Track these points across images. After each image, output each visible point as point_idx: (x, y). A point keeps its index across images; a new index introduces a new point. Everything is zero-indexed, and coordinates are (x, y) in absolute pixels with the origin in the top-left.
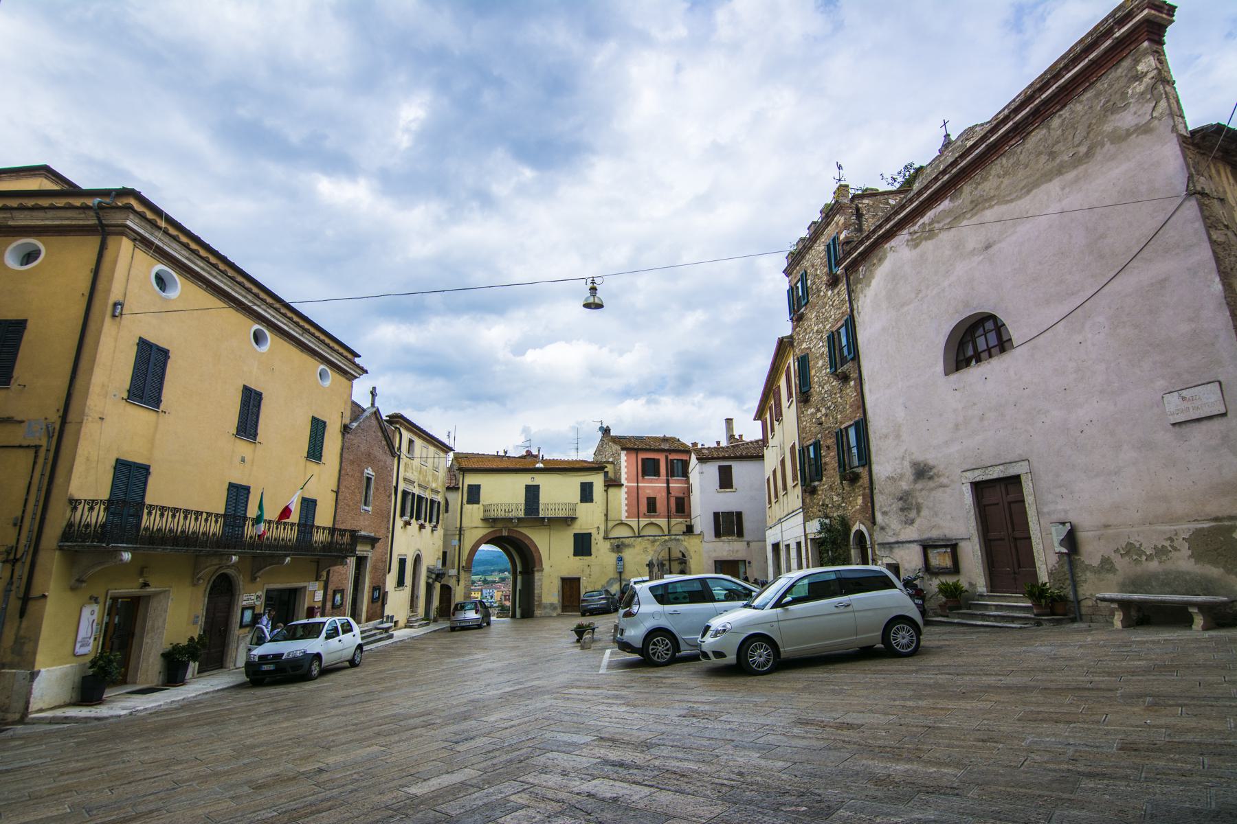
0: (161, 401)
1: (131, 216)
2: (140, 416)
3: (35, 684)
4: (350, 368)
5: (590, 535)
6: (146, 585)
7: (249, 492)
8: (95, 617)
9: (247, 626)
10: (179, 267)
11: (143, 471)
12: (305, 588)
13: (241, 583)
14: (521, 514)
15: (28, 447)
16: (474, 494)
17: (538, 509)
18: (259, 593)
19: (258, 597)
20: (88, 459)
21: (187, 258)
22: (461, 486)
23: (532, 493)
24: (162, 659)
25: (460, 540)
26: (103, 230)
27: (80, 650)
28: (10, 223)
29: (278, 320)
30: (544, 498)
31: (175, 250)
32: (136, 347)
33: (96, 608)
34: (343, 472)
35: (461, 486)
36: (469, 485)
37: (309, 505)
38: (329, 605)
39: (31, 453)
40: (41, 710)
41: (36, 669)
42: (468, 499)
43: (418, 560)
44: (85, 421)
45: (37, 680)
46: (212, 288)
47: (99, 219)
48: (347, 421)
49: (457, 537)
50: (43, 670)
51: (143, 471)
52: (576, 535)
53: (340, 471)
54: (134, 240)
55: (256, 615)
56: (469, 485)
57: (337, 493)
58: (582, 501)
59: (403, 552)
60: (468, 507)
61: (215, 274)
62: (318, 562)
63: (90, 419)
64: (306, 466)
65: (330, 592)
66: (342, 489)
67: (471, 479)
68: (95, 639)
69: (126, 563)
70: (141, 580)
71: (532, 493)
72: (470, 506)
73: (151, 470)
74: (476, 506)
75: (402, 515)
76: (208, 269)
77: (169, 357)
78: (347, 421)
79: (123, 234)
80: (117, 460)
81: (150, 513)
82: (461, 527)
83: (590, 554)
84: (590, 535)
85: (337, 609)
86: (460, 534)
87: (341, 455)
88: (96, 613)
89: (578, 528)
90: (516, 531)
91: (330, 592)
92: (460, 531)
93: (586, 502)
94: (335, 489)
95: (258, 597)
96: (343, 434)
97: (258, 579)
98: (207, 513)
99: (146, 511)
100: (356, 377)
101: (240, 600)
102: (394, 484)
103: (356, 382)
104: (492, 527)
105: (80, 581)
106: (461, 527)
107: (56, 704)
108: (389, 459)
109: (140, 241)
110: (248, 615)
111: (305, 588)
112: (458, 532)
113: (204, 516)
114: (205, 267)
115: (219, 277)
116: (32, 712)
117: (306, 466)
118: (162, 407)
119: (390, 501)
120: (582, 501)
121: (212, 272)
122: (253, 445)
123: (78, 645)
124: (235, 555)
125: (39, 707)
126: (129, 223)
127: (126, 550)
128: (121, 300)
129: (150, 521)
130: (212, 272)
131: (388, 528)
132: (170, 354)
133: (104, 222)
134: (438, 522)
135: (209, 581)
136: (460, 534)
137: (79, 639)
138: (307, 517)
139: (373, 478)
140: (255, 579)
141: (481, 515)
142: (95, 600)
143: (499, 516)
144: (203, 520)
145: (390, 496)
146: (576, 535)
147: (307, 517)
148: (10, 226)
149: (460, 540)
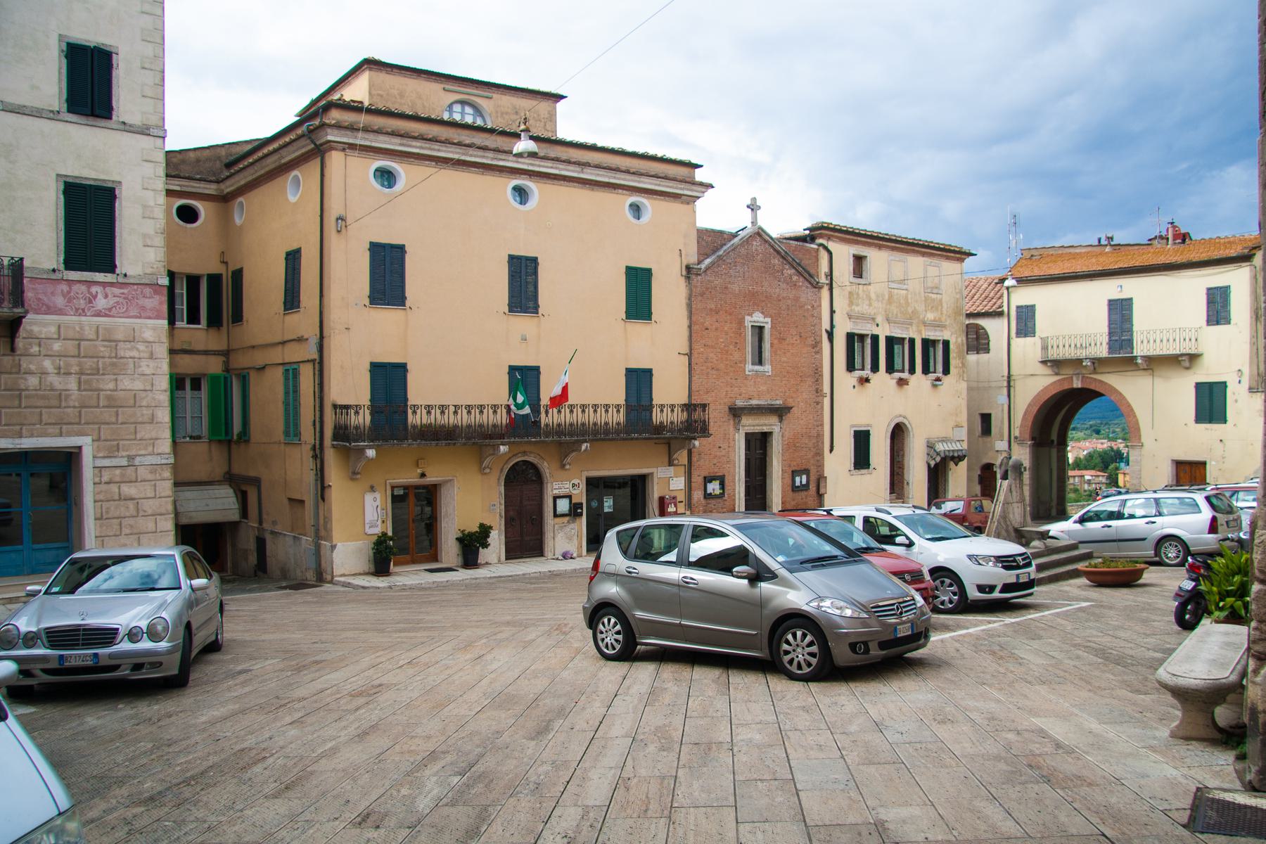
0: (406, 298)
1: (329, 131)
2: (387, 316)
3: (335, 554)
4: (681, 189)
5: (1224, 385)
6: (423, 475)
7: (539, 373)
8: (378, 502)
9: (563, 515)
10: (399, 156)
11: (399, 370)
12: (652, 474)
13: (547, 471)
14: (1103, 352)
15: (308, 361)
16: (1026, 321)
17: (1130, 342)
18: (576, 481)
19: (574, 485)
20: (342, 367)
21: (401, 145)
22: (1005, 309)
23: (1120, 311)
24: (458, 543)
25: (1009, 396)
26: (319, 151)
27: (370, 531)
28: (283, 161)
29: (539, 166)
30: (1141, 323)
31: (385, 142)
32: (368, 253)
33: (378, 495)
34: (695, 328)
35: (1005, 309)
36: (1018, 307)
37: (639, 380)
38: (698, 495)
39: (312, 364)
40: (343, 575)
41: (334, 543)
42: (1017, 329)
43: (898, 433)
44: (332, 334)
45: (335, 551)
46: (442, 162)
47: (313, 142)
48: (692, 258)
49: (1005, 391)
50: (339, 544)
51: (399, 370)
52: (1199, 386)
53: (690, 327)
54: (344, 150)
55: (575, 504)
56: (1018, 307)
57: (690, 355)
58: (1209, 322)
59: (862, 423)
60: (1019, 344)
61: (436, 147)
62: (669, 444)
63: (337, 331)
64: (625, 329)
65: (697, 479)
66: (698, 348)
67: (1023, 296)
68: (383, 522)
69: (372, 459)
70: (419, 471)
71: (1120, 311)
72: (1021, 341)
73: (408, 367)
74: (1029, 339)
75: (851, 367)
76: (427, 146)
77: (406, 252)
78: (692, 258)
79: (332, 149)
80: (371, 363)
81: (414, 412)
82: (1009, 377)
83: (1225, 421)
84: (1224, 385)
85: (716, 503)
86: (1009, 387)
87: (689, 306)
88: (378, 500)
89: (1207, 372)
90: (1092, 378)
91: (697, 479)
92: (1009, 382)
93: (1218, 323)
94: (686, 350)
95: (574, 485)
96: (688, 278)
97: (568, 467)
98: (455, 406)
99: (410, 411)
100: (699, 198)
101: (549, 489)
102: (826, 325)
103: (698, 203)
104: (1057, 374)
105: (354, 473)
106: (1009, 377)
107: (358, 572)
108: (806, 293)
109: (349, 148)
110: (563, 506)
111: (652, 474)
112: (1005, 384)
113: (452, 409)
114: (424, 145)
115: (444, 149)
116: (337, 576)
117: (625, 329)
118: (408, 303)
119: (819, 352)
120: (1209, 322)
121: (433, 147)
122: (536, 319)
123: (367, 526)
124: (503, 445)
125: (342, 573)
126: (330, 138)
127: (370, 447)
128: (342, 213)
129: (414, 419)
130: (433, 147)
131: (818, 391)
132: (407, 249)
133: (318, 143)
134: (946, 371)
135: (502, 470)
136: (1009, 387)
137: (367, 521)
138: (639, 391)
139: (768, 327)
140: (564, 465)
141: (1038, 355)
142: (372, 489)
143: (1068, 356)
144: (451, 413)
145: (817, 345)
146: (1199, 386)
147: (639, 391)
148: (285, 164)
149: (1009, 396)
